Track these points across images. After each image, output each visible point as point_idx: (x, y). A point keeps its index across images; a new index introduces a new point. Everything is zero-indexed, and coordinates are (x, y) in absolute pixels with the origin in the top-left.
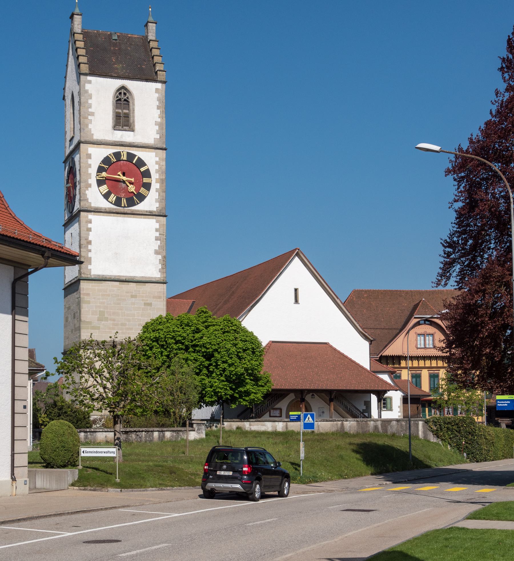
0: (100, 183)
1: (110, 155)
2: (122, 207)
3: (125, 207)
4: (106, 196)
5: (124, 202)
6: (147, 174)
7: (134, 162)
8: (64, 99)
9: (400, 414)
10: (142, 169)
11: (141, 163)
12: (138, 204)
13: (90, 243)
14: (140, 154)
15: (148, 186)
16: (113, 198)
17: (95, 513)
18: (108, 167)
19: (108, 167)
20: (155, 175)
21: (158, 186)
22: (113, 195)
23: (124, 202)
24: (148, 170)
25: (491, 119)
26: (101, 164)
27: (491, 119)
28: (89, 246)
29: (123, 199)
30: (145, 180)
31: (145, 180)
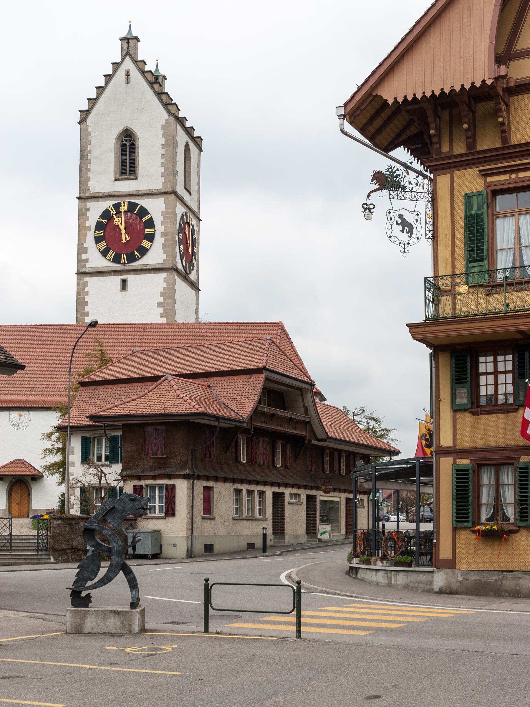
0: (98, 240)
1: (109, 207)
2: (122, 264)
3: (124, 263)
4: (104, 253)
5: (124, 258)
6: (150, 223)
7: (135, 212)
8: (112, 664)
9: (139, 523)
10: (144, 219)
11: (144, 212)
12: (139, 259)
13: (89, 170)
14: (141, 202)
15: (151, 238)
16: (111, 254)
17: (22, 610)
18: (106, 221)
19: (106, 221)
20: (159, 228)
21: (162, 240)
22: (111, 251)
23: (124, 258)
24: (151, 220)
25: (42, 516)
26: (99, 218)
27: (42, 516)
28: (89, 173)
29: (122, 255)
30: (148, 231)
31: (148, 231)
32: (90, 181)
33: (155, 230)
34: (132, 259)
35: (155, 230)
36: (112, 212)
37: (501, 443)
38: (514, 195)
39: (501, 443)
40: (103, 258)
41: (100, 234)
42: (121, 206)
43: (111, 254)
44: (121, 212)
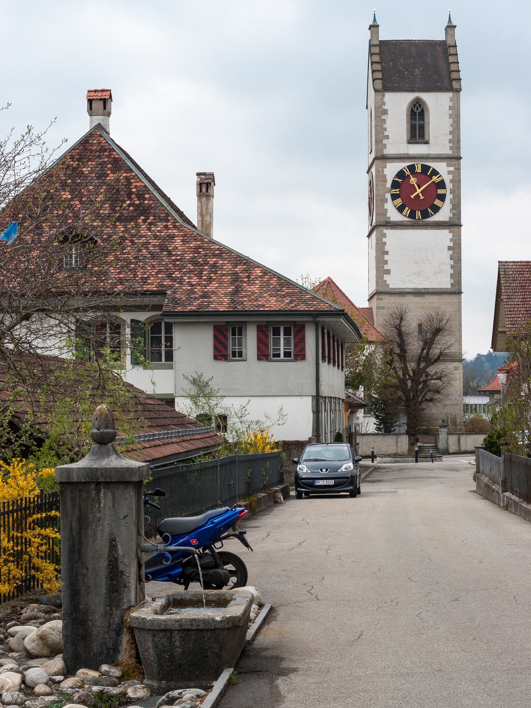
4: (400, 209)
5: (418, 214)
22: (407, 208)
23: (418, 214)
34: (426, 215)
41: (396, 191)
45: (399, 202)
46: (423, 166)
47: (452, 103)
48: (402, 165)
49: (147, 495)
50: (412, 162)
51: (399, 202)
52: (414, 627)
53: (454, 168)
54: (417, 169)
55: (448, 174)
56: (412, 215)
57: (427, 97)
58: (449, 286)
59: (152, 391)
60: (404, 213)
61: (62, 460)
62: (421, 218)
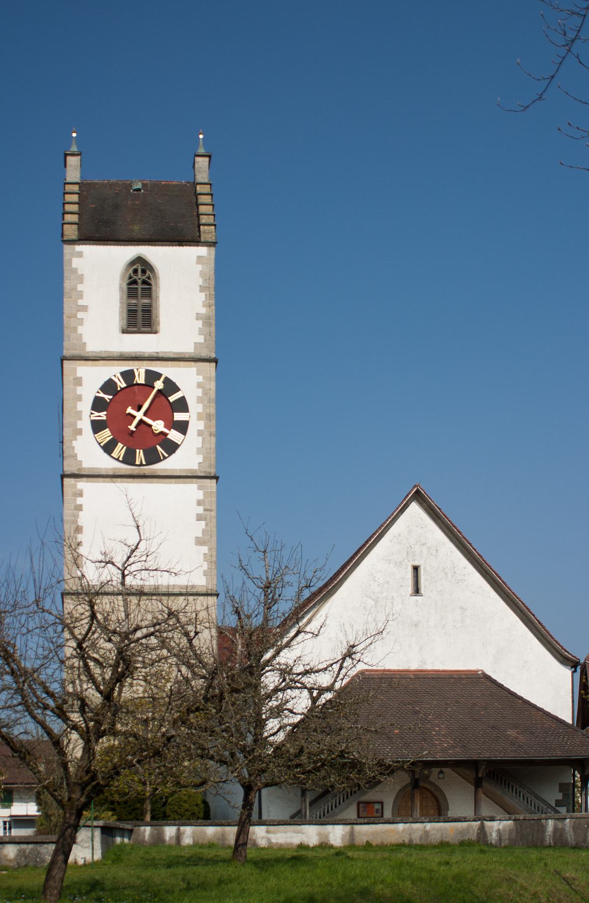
3: (141, 465)
4: (108, 448)
5: (140, 455)
14: (167, 371)
16: (120, 450)
18: (111, 397)
22: (120, 445)
23: (140, 455)
24: (183, 400)
30: (103, 416)
31: (103, 416)
32: (82, 325)
33: (90, 416)
34: (153, 458)
35: (90, 416)
36: (119, 383)
37: (374, 883)
38: (29, 814)
39: (374, 883)
40: (106, 455)
41: (100, 416)
42: (159, 379)
43: (120, 450)
44: (154, 388)
45: (106, 435)
46: (148, 372)
47: (201, 492)
48: (113, 372)
49: (228, 853)
50: (129, 366)
51: (106, 435)
52: (222, 756)
53: (204, 378)
54: (137, 378)
55: (198, 520)
56: (129, 459)
57: (153, 253)
58: (196, 467)
59: (28, 807)
60: (115, 454)
61: (517, 876)
62: (144, 463)
